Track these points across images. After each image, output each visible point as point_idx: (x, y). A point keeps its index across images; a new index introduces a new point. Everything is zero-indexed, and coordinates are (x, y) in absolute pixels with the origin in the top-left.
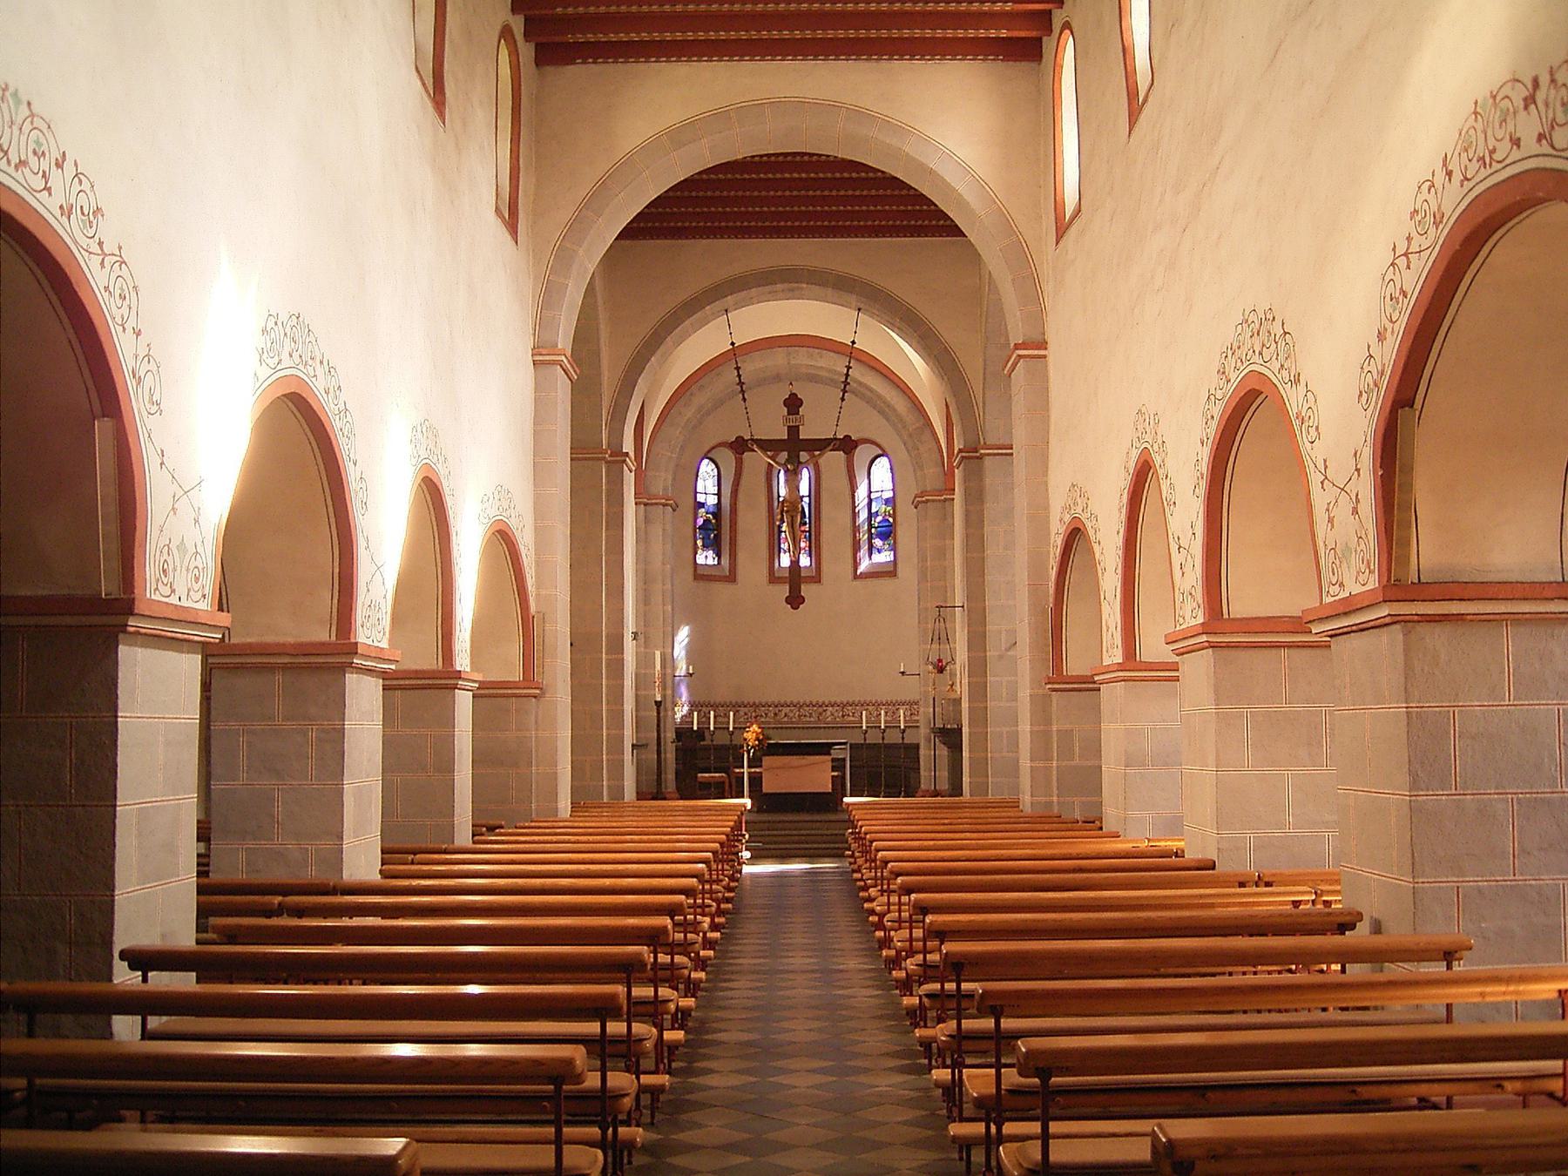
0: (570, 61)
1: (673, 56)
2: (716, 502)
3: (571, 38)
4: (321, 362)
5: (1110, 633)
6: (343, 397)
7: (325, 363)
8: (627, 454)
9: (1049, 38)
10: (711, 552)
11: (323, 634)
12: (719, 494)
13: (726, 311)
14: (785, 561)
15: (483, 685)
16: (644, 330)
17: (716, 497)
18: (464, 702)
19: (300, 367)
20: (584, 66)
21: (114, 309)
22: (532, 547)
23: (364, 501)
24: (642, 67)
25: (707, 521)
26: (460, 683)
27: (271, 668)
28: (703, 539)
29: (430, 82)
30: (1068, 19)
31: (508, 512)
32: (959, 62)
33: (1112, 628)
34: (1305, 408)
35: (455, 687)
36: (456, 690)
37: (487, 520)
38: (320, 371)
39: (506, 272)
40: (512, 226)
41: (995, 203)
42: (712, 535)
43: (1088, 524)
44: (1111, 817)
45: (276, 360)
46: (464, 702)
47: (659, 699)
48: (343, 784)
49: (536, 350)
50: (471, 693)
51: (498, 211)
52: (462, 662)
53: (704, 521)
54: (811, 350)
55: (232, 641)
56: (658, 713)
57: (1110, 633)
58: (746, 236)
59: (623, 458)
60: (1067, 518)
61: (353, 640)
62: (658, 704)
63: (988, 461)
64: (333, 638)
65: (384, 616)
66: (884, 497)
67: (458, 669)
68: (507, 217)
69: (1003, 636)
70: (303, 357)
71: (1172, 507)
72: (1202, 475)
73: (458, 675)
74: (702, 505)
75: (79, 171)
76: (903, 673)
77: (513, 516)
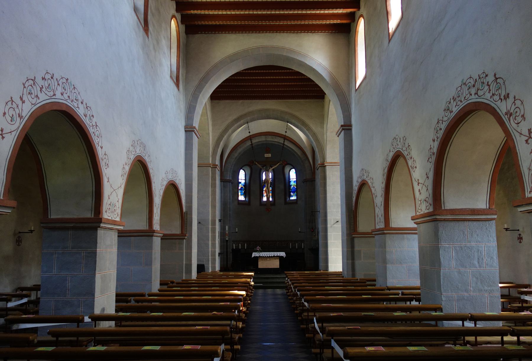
0: (196, 33)
1: (230, 31)
2: (244, 182)
3: (197, 23)
4: (82, 103)
5: (379, 218)
6: (94, 120)
7: (84, 103)
8: (217, 165)
9: (354, 23)
10: (243, 196)
11: (89, 215)
12: (245, 180)
13: (248, 122)
14: (265, 199)
15: (165, 235)
16: (223, 127)
17: (244, 180)
18: (157, 242)
19: (69, 101)
20: (201, 35)
21: (96, 140)
22: (184, 190)
23: (107, 163)
24: (221, 35)
25: (242, 188)
26: (154, 234)
27: (67, 229)
28: (241, 193)
29: (142, 17)
30: (362, 13)
31: (175, 178)
32: (323, 33)
33: (380, 216)
34: (513, 107)
35: (152, 236)
36: (153, 237)
37: (167, 180)
38: (80, 105)
39: (175, 98)
40: (177, 85)
41: (335, 79)
42: (243, 192)
43: (369, 182)
44: (444, 305)
45: (52, 93)
46: (157, 242)
47: (227, 239)
48: (95, 274)
49: (186, 127)
50: (160, 238)
51: (171, 77)
52: (156, 227)
53: (241, 187)
54: (273, 136)
55: (51, 218)
56: (227, 244)
57: (379, 218)
58: (254, 99)
59: (216, 166)
60: (360, 180)
61: (101, 217)
62: (227, 241)
63: (327, 167)
64: (93, 216)
65: (118, 209)
66: (294, 180)
67: (154, 229)
68: (175, 82)
69: (332, 221)
70: (71, 97)
71: (414, 169)
72: (434, 154)
73: (154, 231)
74: (240, 183)
75: (87, 106)
76: (300, 232)
77: (177, 179)
